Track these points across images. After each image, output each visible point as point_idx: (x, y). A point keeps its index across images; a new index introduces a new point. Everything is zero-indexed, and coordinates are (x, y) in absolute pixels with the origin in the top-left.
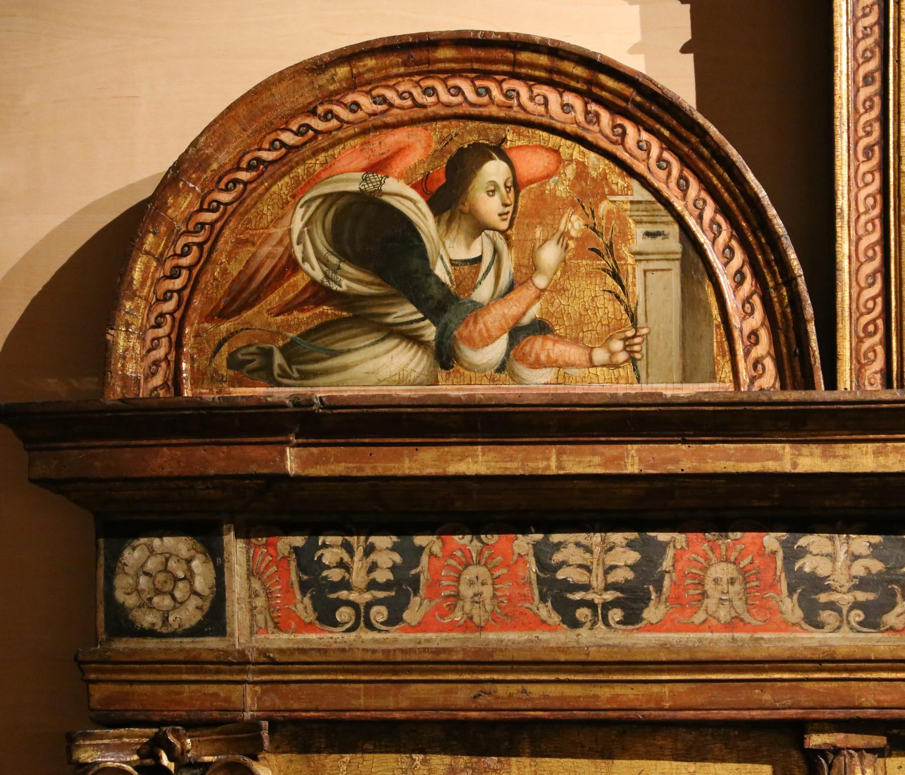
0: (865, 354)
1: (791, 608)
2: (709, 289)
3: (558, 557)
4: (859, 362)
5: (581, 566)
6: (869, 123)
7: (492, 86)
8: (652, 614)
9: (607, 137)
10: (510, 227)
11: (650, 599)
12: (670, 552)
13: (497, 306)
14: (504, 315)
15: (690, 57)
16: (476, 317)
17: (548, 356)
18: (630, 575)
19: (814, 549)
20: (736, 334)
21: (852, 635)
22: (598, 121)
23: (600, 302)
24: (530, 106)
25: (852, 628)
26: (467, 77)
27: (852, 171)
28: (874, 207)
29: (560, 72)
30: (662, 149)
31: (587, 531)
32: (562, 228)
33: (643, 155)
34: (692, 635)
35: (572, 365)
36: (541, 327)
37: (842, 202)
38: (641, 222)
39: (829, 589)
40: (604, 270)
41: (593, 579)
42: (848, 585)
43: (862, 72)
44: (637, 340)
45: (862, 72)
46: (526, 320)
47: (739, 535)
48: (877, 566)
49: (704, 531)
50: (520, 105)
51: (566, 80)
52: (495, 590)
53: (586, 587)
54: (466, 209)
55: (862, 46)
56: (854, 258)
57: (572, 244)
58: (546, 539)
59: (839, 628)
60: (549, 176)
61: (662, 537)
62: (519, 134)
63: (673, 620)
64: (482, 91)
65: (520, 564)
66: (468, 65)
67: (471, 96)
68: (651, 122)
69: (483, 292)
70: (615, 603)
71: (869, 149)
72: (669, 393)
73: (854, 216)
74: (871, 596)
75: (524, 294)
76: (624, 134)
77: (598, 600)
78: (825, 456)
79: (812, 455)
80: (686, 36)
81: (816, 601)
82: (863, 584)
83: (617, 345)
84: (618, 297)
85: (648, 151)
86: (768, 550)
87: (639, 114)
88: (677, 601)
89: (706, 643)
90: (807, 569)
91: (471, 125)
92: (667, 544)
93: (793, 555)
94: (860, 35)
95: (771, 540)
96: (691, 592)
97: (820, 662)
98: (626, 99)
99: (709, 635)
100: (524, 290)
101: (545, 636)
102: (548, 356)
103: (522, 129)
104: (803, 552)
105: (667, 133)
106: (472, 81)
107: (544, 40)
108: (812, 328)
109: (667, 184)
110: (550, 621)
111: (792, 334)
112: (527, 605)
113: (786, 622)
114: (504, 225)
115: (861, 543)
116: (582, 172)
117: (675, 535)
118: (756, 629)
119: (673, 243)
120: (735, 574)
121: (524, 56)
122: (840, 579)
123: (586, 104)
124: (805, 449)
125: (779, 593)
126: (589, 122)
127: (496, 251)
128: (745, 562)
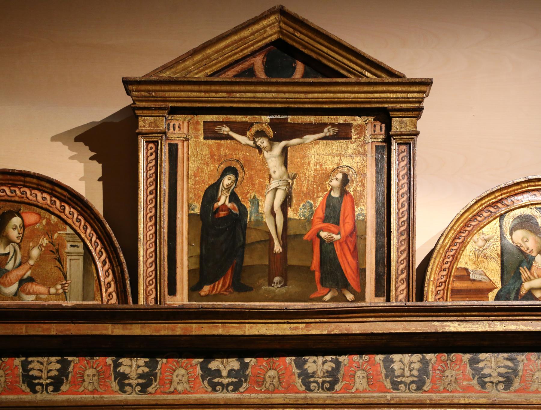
0: (149, 293)
1: (115, 386)
2: (93, 267)
3: (30, 366)
4: (146, 294)
5: (38, 370)
6: (151, 208)
7: (17, 190)
8: (64, 388)
9: (58, 210)
10: (21, 241)
11: (63, 382)
12: (72, 364)
13: (15, 271)
14: (17, 275)
15: (101, 182)
16: (6, 275)
17: (33, 290)
18: (57, 373)
19: (124, 363)
20: (102, 283)
21: (136, 395)
22: (55, 204)
23: (53, 270)
24: (30, 197)
25: (136, 393)
26: (7, 186)
27: (145, 225)
28: (152, 238)
29: (41, 186)
30: (78, 215)
31: (42, 356)
32: (40, 242)
33: (71, 217)
34: (78, 396)
35: (42, 294)
36: (31, 280)
37: (141, 236)
38: (69, 241)
39: (129, 378)
40: (55, 259)
41: (43, 375)
42: (136, 377)
43: (149, 190)
44: (66, 285)
45: (149, 190)
46: (25, 277)
47: (98, 358)
48: (146, 370)
49: (85, 356)
50: (27, 197)
51: (44, 189)
52: (6, 379)
53: (40, 378)
54: (5, 235)
55: (149, 181)
56: (145, 257)
57: (43, 249)
58: (26, 360)
59: (132, 393)
60: (36, 223)
61: (70, 359)
62: (26, 208)
63: (71, 390)
64: (13, 191)
65: (16, 369)
66: (7, 182)
67: (8, 193)
68: (74, 205)
69: (10, 266)
70: (50, 384)
71: (151, 218)
72: (64, 305)
73: (145, 242)
74: (143, 381)
75: (25, 267)
76: (64, 209)
77: (44, 382)
78: (123, 329)
79: (119, 328)
80: (100, 175)
81: (124, 383)
82: (141, 376)
83: (59, 287)
84: (60, 269)
85: (73, 215)
86: (108, 364)
87: (70, 202)
88: (74, 383)
89: (83, 399)
90: (121, 371)
91: (8, 204)
92: (71, 361)
93: (117, 365)
94: (148, 177)
95: (109, 360)
96: (79, 379)
97: (123, 406)
98: (65, 196)
99: (85, 396)
100: (25, 266)
101: (24, 396)
102: (33, 290)
103: (27, 206)
104: (121, 364)
105: (79, 209)
106: (9, 187)
107: (34, 173)
108: (128, 282)
109: (79, 227)
110: (26, 391)
111: (122, 284)
112: (17, 385)
113: (113, 391)
114: (19, 241)
115: (141, 361)
116: (48, 223)
117: (74, 358)
118: (102, 393)
119: (81, 250)
120: (95, 373)
121: (28, 179)
122: (133, 375)
123: (51, 197)
124: (117, 326)
125: (111, 380)
126: (52, 204)
127: (15, 251)
128: (99, 368)
